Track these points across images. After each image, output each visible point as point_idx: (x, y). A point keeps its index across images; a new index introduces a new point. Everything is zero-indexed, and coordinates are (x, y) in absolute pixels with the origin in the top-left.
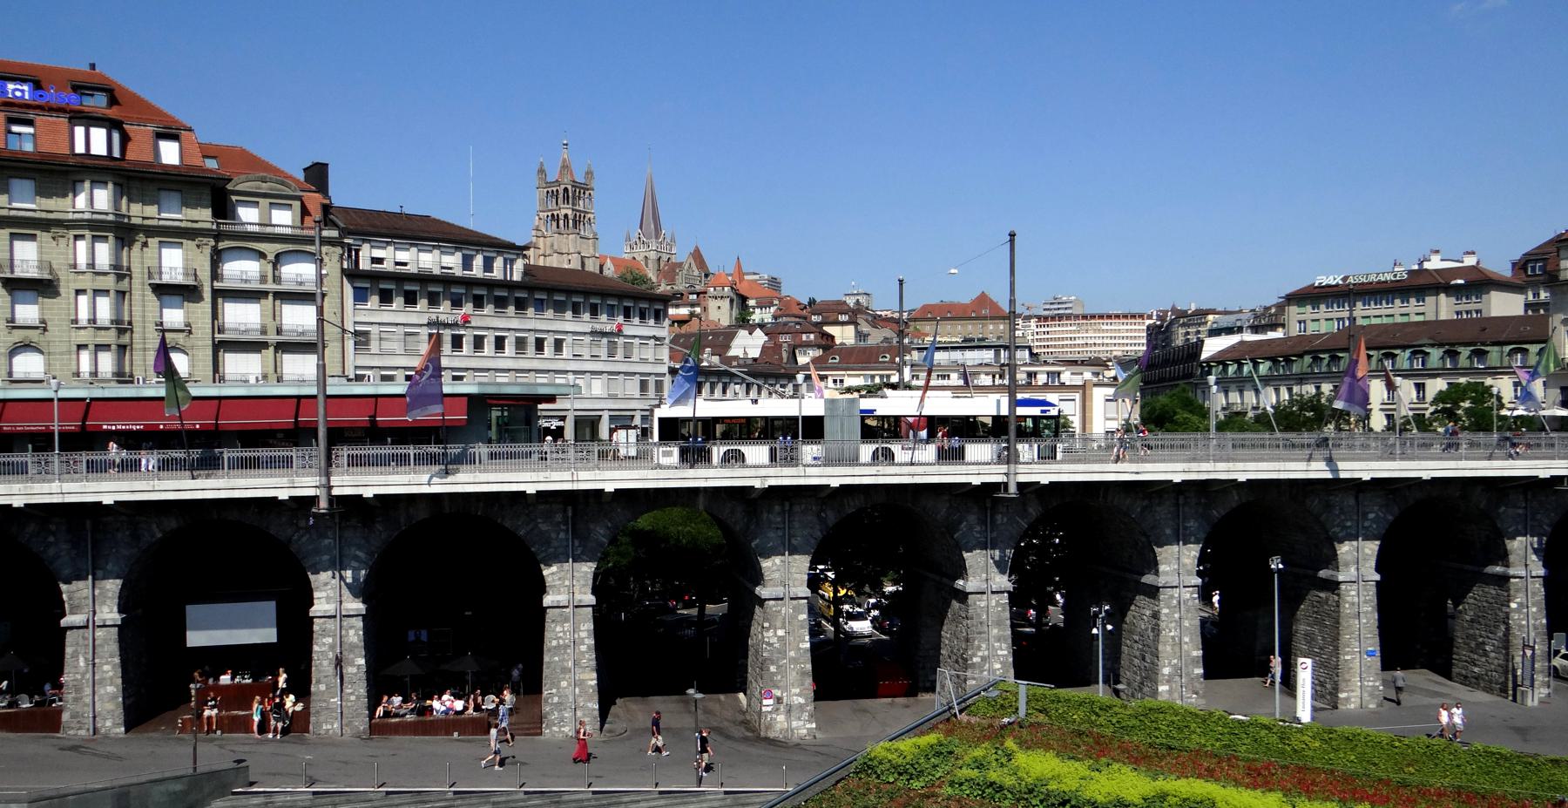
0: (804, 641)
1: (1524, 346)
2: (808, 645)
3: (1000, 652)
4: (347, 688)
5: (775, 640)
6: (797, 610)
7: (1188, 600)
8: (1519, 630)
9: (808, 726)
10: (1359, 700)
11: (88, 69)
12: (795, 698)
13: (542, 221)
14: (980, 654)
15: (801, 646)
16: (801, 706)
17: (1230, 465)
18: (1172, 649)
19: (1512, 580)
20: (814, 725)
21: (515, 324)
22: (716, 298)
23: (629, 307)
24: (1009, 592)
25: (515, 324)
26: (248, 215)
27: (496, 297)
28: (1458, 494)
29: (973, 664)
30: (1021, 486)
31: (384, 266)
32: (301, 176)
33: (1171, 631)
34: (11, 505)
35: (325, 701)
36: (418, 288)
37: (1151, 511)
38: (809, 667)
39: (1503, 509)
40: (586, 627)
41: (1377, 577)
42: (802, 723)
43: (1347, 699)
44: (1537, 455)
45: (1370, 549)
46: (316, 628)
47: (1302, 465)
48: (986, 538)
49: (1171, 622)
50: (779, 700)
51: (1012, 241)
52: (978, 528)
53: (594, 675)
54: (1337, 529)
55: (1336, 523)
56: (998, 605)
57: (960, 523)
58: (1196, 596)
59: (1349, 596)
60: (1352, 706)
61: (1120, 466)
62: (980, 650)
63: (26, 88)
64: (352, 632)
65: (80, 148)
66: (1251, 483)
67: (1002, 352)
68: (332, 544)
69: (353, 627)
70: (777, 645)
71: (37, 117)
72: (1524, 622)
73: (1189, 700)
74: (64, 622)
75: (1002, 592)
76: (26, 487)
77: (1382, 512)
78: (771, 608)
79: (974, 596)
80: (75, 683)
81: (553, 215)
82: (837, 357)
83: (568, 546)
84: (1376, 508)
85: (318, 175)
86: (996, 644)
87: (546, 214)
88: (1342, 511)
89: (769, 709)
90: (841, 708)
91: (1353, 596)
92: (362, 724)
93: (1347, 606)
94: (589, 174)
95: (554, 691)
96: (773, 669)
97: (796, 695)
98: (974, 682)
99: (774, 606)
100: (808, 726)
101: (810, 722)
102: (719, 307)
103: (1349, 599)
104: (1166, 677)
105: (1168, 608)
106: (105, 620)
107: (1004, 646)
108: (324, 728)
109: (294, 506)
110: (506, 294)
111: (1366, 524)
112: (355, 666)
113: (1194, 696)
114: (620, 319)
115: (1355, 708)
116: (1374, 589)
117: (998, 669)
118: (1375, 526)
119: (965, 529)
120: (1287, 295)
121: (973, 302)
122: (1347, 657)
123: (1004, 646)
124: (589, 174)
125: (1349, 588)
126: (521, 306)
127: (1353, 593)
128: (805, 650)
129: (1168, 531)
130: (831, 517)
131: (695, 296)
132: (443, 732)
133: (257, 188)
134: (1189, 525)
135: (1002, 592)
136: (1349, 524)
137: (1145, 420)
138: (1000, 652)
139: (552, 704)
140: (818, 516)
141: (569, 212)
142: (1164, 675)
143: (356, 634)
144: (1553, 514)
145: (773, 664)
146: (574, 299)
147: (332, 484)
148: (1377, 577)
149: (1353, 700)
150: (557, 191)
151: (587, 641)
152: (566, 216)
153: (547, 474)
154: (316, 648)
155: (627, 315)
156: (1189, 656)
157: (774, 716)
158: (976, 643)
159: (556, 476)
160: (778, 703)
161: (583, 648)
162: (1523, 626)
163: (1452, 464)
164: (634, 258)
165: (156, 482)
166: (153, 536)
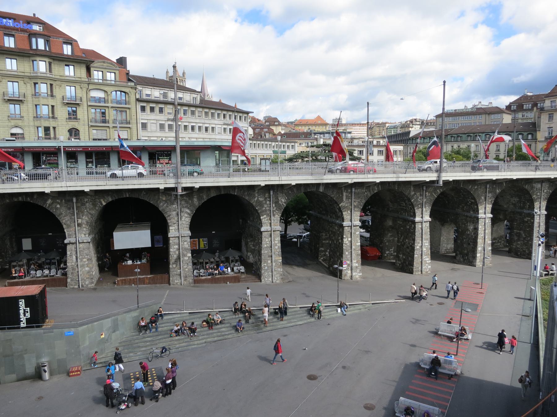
0: (358, 242)
1: (522, 133)
2: (359, 244)
4: (482, 237)
9: (359, 274)
11: (33, 16)
12: (355, 264)
15: (357, 244)
16: (357, 267)
20: (361, 274)
24: (429, 222)
26: (97, 75)
29: (417, 249)
30: (185, 189)
32: (115, 61)
34: (44, 192)
35: (175, 271)
38: (360, 252)
40: (277, 239)
41: (546, 213)
42: (357, 273)
46: (171, 242)
47: (533, 173)
48: (423, 201)
50: (348, 265)
52: (420, 198)
53: (281, 258)
54: (534, 196)
58: (490, 221)
61: (407, 175)
63: (10, 21)
64: (185, 243)
65: (34, 47)
66: (382, 183)
68: (177, 207)
69: (186, 241)
71: (16, 34)
74: (66, 241)
75: (427, 222)
76: (51, 184)
79: (265, 233)
80: (72, 267)
83: (271, 207)
85: (122, 62)
89: (345, 268)
92: (190, 280)
95: (265, 264)
97: (355, 263)
100: (359, 274)
101: (359, 273)
106: (83, 240)
107: (427, 242)
108: (176, 282)
112: (187, 257)
116: (544, 217)
123: (427, 242)
128: (358, 246)
130: (196, 202)
132: (223, 282)
133: (102, 66)
135: (427, 222)
137: (404, 160)
138: (426, 244)
139: (265, 270)
142: (479, 250)
143: (188, 244)
145: (347, 251)
146: (212, 111)
148: (546, 213)
151: (278, 245)
153: (269, 178)
154: (171, 250)
157: (347, 271)
159: (272, 178)
161: (277, 247)
165: (107, 182)
166: (102, 204)
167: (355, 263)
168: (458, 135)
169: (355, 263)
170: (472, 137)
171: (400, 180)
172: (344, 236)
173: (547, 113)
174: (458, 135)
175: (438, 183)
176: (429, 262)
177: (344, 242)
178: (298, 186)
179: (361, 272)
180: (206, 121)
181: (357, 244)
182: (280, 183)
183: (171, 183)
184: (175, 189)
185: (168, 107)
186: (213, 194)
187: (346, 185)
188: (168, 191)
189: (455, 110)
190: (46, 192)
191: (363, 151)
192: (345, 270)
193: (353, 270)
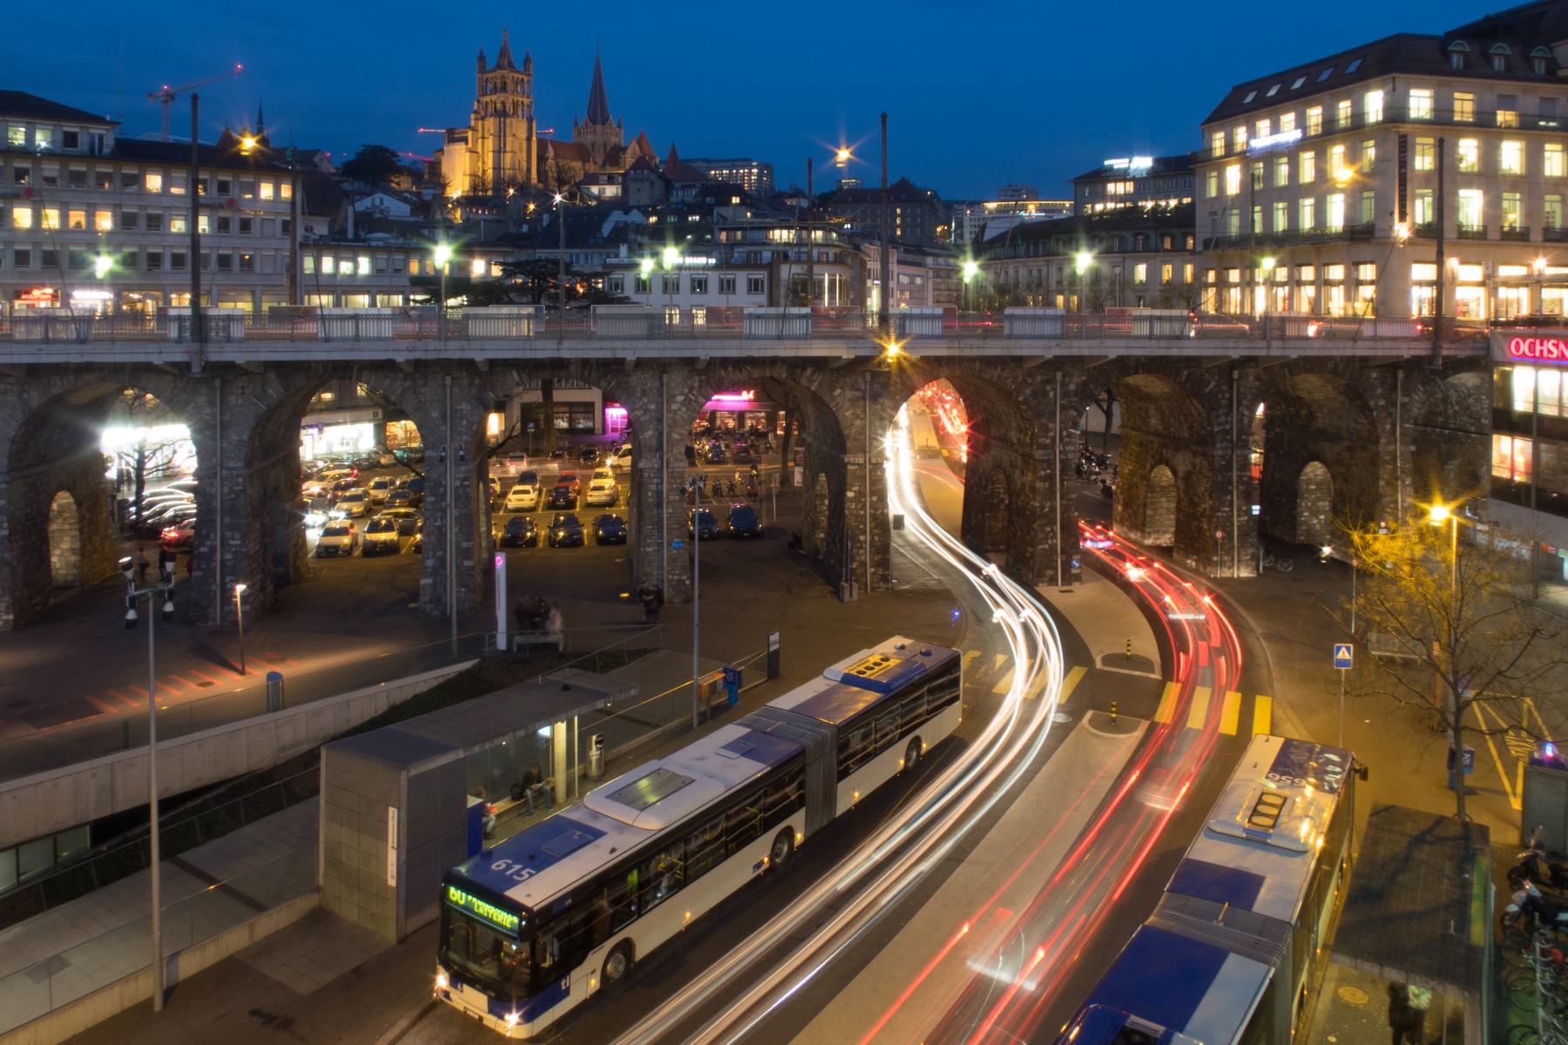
3: (232, 542)
22: (636, 180)
27: (71, 172)
28: (784, 375)
29: (200, 554)
33: (435, 521)
37: (415, 393)
39: (838, 392)
44: (1392, 344)
45: (679, 434)
51: (884, 122)
52: (208, 410)
55: (637, 406)
72: (862, 512)
88: (644, 393)
98: (200, 573)
101: (7, 613)
102: (639, 190)
105: (434, 496)
110: (84, 169)
118: (684, 409)
120: (1076, 179)
122: (648, 549)
134: (460, 408)
138: (232, 542)
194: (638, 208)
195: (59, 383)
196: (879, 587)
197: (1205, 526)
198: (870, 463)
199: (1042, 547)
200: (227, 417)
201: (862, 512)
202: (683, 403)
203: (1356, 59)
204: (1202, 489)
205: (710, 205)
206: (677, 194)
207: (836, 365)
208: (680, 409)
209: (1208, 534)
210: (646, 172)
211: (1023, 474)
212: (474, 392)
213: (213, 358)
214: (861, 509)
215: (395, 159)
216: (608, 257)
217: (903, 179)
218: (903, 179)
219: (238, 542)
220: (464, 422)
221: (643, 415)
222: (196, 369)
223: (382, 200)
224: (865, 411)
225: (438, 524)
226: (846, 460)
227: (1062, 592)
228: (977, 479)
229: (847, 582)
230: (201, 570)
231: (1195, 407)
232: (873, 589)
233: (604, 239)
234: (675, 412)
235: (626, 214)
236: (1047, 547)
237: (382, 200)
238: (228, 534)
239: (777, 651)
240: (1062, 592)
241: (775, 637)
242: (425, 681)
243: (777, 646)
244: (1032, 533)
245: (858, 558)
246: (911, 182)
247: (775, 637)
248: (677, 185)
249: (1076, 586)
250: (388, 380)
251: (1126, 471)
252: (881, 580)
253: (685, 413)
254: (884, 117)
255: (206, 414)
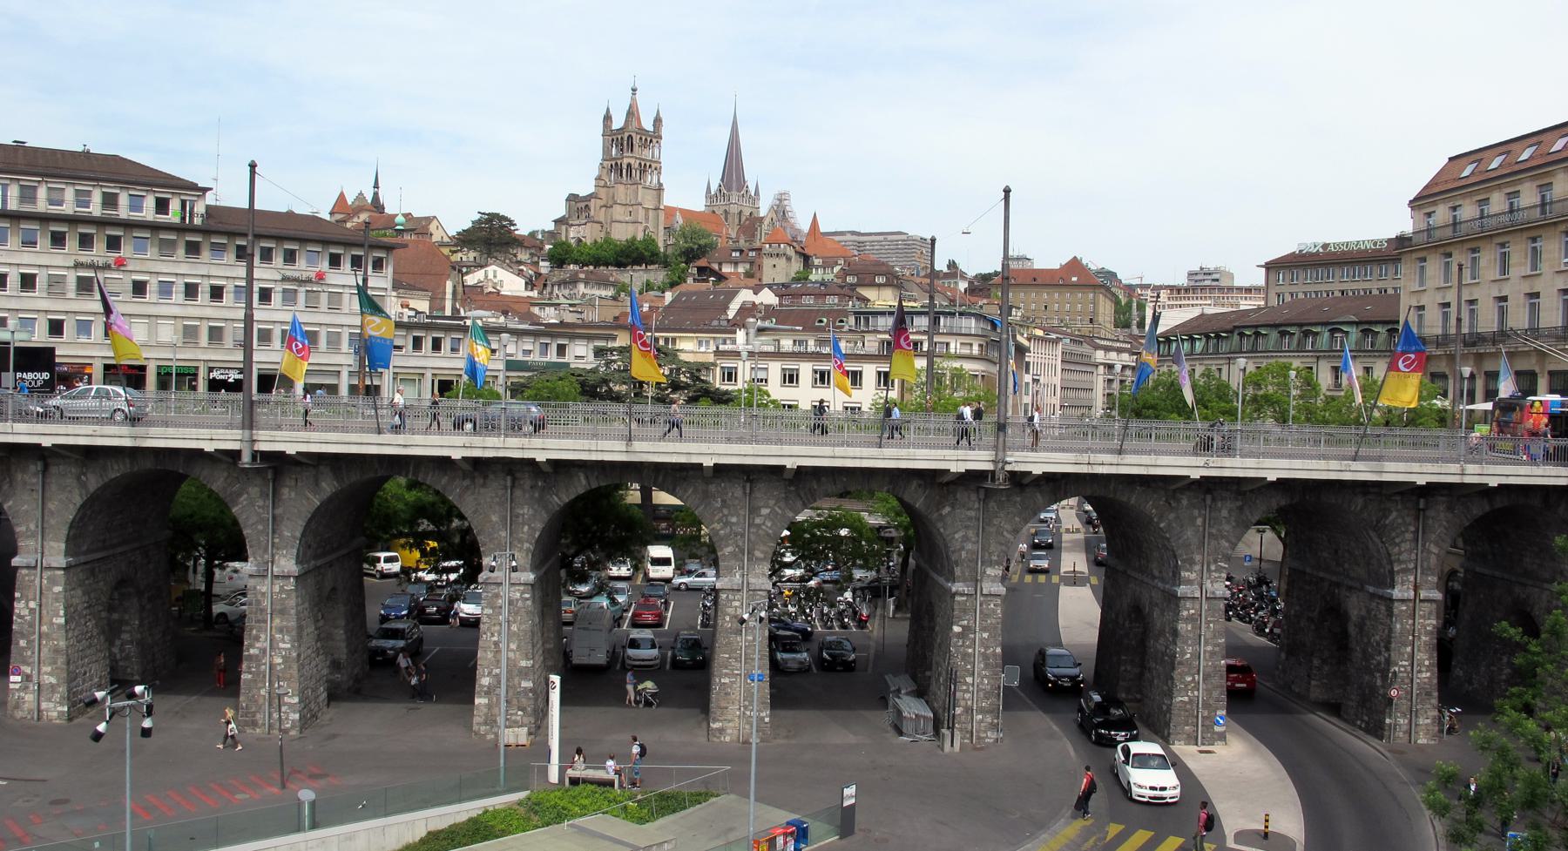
0: (58, 616)
5: (26, 612)
6: (53, 582)
7: (517, 600)
8: (962, 660)
9: (60, 709)
10: (736, 732)
12: (46, 677)
13: (605, 171)
14: (257, 645)
17: (194, 432)
18: (494, 657)
19: (958, 598)
21: (183, 269)
23: (361, 257)
25: (183, 269)
29: (250, 656)
31: (64, 207)
33: (493, 635)
36: (8, 225)
39: (947, 510)
43: (721, 731)
45: (762, 552)
49: (494, 625)
50: (28, 678)
52: (261, 503)
55: (717, 518)
56: (282, 590)
57: (240, 495)
59: (731, 607)
60: (728, 739)
62: (258, 641)
67: (942, 320)
70: (28, 618)
72: (970, 650)
73: (513, 718)
77: (779, 507)
78: (23, 578)
81: (616, 164)
82: (825, 320)
84: (772, 502)
86: (277, 636)
87: (609, 163)
89: (17, 686)
90: (788, 715)
91: (736, 607)
93: (728, 619)
94: (658, 121)
96: (23, 643)
97: (49, 674)
98: (250, 676)
99: (27, 575)
100: (60, 709)
101: (61, 704)
103: (730, 610)
104: (485, 689)
105: (491, 608)
109: (466, 467)
110: (225, 242)
111: (758, 521)
113: (520, 713)
114: (324, 265)
115: (732, 741)
117: (280, 664)
119: (245, 503)
120: (1266, 264)
121: (1063, 267)
124: (658, 121)
125: (731, 597)
126: (193, 249)
127: (737, 604)
128: (59, 626)
129: (494, 518)
130: (94, 482)
131: (738, 254)
136: (734, 520)
140: (78, 478)
141: (632, 161)
144: (1017, 519)
147: (255, 438)
149: (729, 731)
150: (622, 138)
152: (629, 165)
155: (335, 261)
156: (515, 666)
157: (22, 694)
158: (254, 632)
160: (27, 681)
162: (969, 655)
163: (827, 451)
164: (714, 212)
167: (46, 673)
168: (1305, 328)
169: (46, 673)
170: (1296, 338)
171: (1468, 480)
172: (17, 595)
173: (1415, 256)
174: (1305, 328)
175: (993, 479)
176: (293, 701)
177: (17, 611)
178: (1282, 484)
179: (66, 702)
180: (214, 271)
181: (54, 620)
182: (1091, 472)
183: (979, 459)
184: (235, 455)
185: (22, 226)
186: (148, 464)
187: (1179, 485)
188: (973, 478)
189: (1325, 246)
190: (207, 449)
191: (736, 368)
192: (17, 690)
193: (42, 695)
194: (770, 286)
195: (116, 467)
196: (987, 737)
197: (1379, 682)
198: (982, 594)
199: (1180, 699)
200: (279, 511)
201: (970, 650)
202: (768, 517)
203: (1501, 154)
204: (1378, 638)
205: (852, 285)
206: (817, 273)
207: (946, 479)
208: (764, 524)
209: (1381, 692)
210: (782, 246)
211: (1163, 611)
212: (537, 495)
213: (263, 447)
214: (969, 647)
215: (512, 228)
216: (724, 343)
217: (1075, 257)
218: (1075, 257)
219: (289, 646)
220: (526, 528)
221: (722, 529)
222: (246, 458)
223: (495, 272)
224: (978, 535)
225: (495, 639)
226: (954, 589)
227: (1201, 752)
228: (1113, 616)
229: (948, 728)
230: (250, 673)
231: (1373, 542)
232: (979, 738)
233: (728, 321)
234: (759, 526)
235: (756, 293)
236: (1186, 699)
237: (495, 272)
238: (278, 636)
239: (852, 806)
240: (1201, 752)
241: (850, 791)
242: (467, 811)
243: (853, 801)
244: (1170, 682)
245: (963, 703)
246: (1084, 262)
247: (850, 791)
248: (817, 262)
249: (1218, 748)
250: (446, 478)
251: (1293, 612)
252: (990, 729)
253: (770, 528)
254: (1007, 191)
255: (259, 507)
